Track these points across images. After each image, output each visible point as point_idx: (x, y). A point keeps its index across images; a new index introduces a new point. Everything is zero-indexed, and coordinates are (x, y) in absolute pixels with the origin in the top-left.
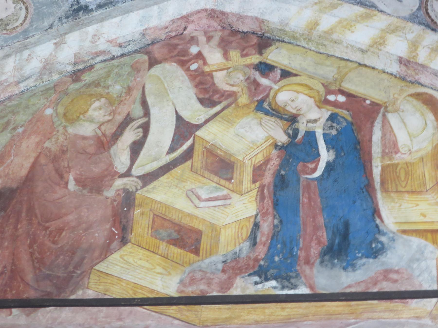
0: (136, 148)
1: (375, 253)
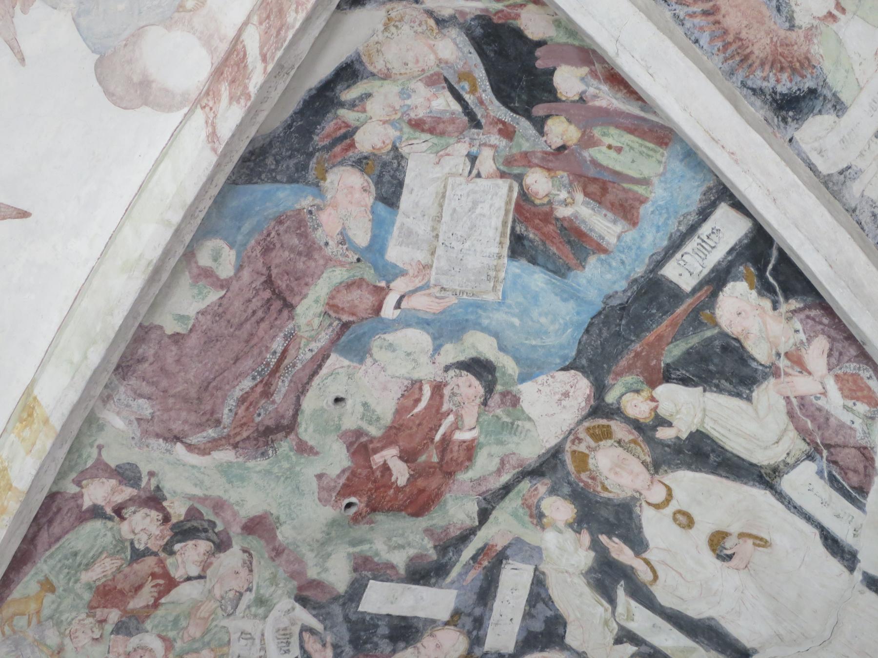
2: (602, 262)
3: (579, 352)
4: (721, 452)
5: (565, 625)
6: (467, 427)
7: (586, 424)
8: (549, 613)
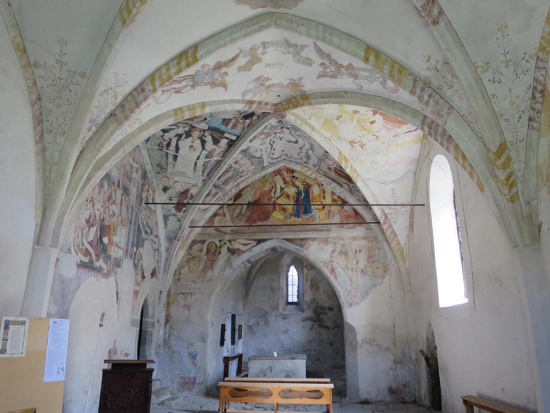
0: (275, 192)
1: (310, 213)
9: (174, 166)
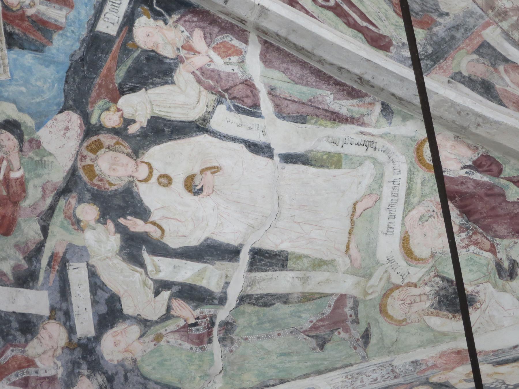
2: (61, 35)
3: (66, 97)
4: (170, 124)
5: (119, 300)
6: (16, 169)
7: (85, 144)
8: (107, 296)
9: (319, 264)
